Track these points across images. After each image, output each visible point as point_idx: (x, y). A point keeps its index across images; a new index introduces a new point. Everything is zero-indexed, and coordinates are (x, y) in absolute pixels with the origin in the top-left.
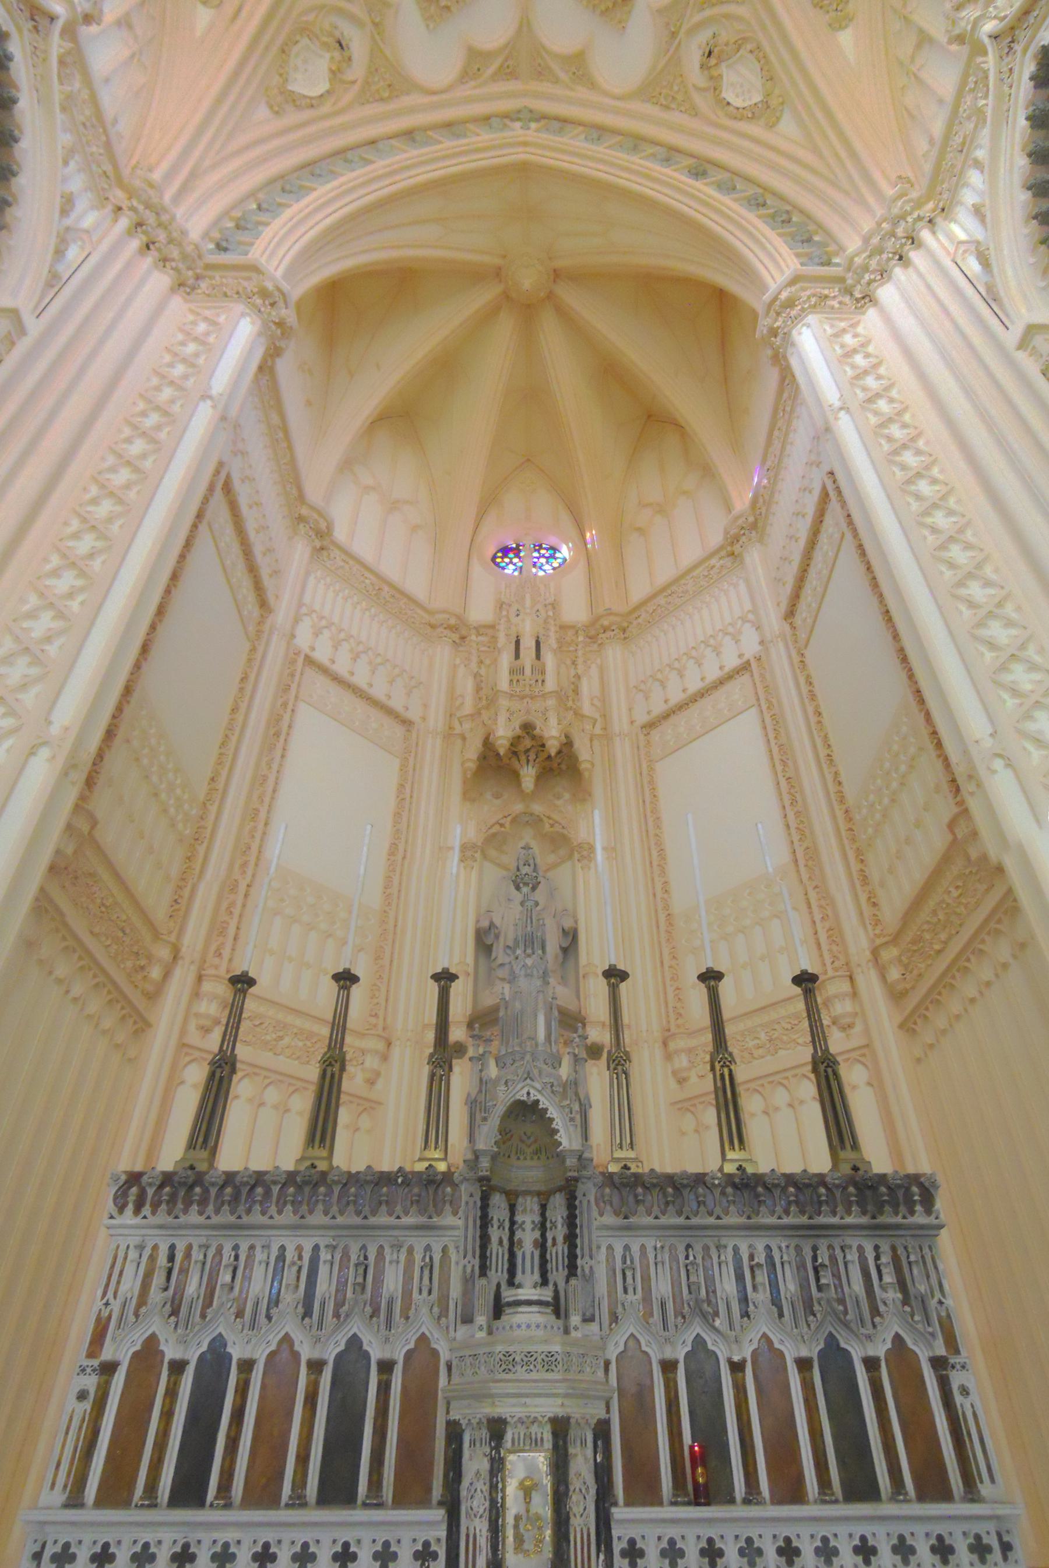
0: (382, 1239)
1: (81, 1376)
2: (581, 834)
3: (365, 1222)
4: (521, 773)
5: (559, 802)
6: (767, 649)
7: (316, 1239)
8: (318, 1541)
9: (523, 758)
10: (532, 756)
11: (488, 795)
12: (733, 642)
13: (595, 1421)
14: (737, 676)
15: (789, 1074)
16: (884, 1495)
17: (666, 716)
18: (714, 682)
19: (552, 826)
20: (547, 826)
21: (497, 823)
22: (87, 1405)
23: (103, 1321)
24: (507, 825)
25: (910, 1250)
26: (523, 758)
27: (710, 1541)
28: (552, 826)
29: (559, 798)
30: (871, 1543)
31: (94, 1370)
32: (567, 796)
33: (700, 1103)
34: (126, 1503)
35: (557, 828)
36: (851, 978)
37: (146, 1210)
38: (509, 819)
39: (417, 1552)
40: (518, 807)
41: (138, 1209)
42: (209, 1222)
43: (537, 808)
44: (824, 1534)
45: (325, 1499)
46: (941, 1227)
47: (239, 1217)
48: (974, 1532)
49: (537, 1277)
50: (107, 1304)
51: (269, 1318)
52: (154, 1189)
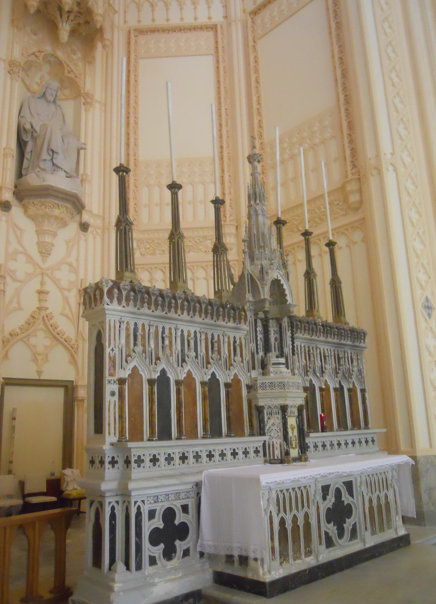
0: (219, 331)
1: (110, 384)
2: (88, 87)
3: (215, 323)
4: (60, 25)
5: (75, 57)
6: (229, 24)
7: (196, 328)
8: (188, 452)
9: (65, 16)
10: (72, 17)
11: (28, 29)
12: (207, 6)
13: (298, 406)
14: (205, 30)
15: (195, 264)
16: (349, 428)
17: (153, 31)
18: (191, 26)
19: (69, 72)
20: (66, 72)
21: (33, 54)
22: (116, 398)
23: (112, 358)
24: (41, 58)
25: (359, 355)
26: (65, 16)
27: (169, 455)
28: (69, 72)
29: (74, 54)
30: (248, 450)
31: (115, 382)
32: (79, 55)
33: (141, 268)
34: (169, 438)
35: (72, 75)
36: (237, 227)
37: (124, 303)
38: (43, 54)
39: (254, 451)
40: (48, 49)
41: (120, 302)
42: (153, 313)
43: (60, 54)
44: (140, 454)
45: (160, 438)
46: (366, 348)
47: (93, 309)
48: (233, 448)
49: (277, 353)
50: (113, 350)
51: (127, 362)
52: (126, 292)
